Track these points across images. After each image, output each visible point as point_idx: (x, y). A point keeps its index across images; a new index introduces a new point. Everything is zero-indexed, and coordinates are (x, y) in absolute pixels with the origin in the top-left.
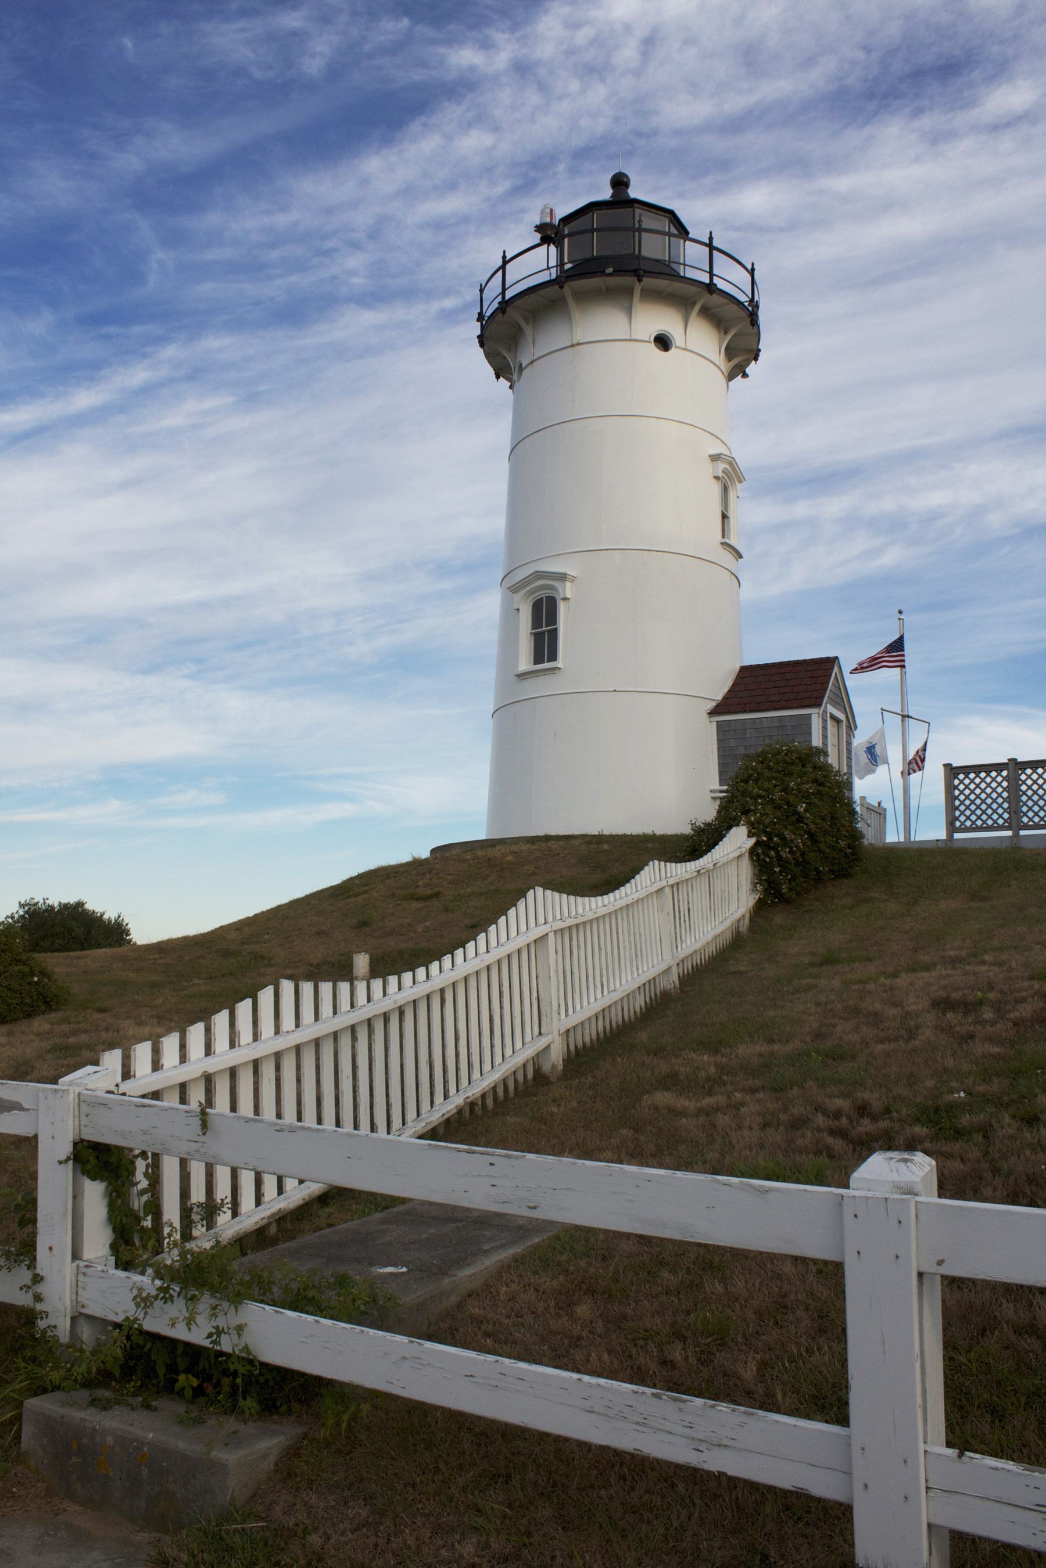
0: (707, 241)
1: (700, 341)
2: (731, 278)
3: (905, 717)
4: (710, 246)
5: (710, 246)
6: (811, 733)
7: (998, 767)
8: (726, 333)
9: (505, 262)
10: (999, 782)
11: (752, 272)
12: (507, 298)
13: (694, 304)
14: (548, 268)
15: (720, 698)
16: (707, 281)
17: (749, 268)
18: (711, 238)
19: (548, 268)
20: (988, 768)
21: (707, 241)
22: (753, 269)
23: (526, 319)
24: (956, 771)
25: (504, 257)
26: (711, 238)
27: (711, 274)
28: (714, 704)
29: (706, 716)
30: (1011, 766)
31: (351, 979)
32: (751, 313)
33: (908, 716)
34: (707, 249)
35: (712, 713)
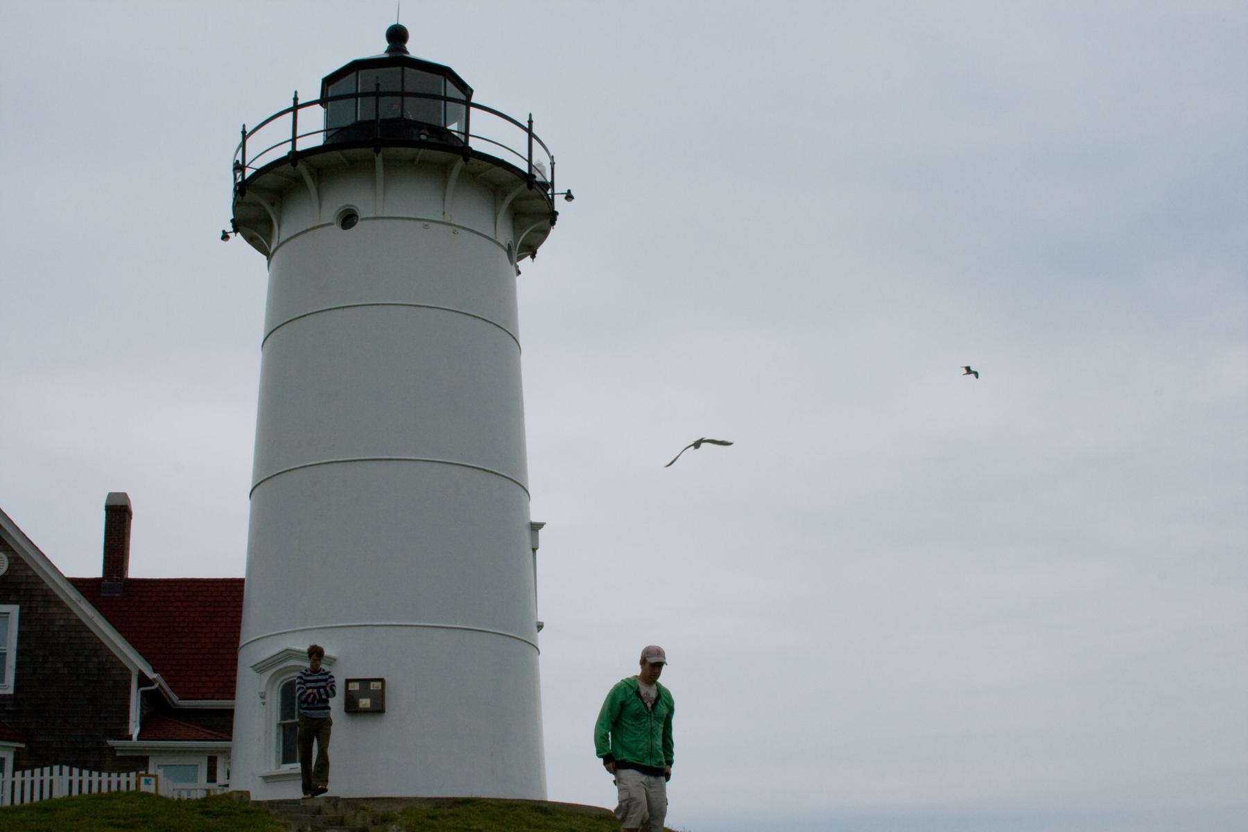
5: (529, 131)
9: (296, 108)
12: (299, 148)
13: (505, 195)
16: (526, 171)
18: (530, 122)
25: (296, 99)
26: (530, 122)
27: (530, 161)
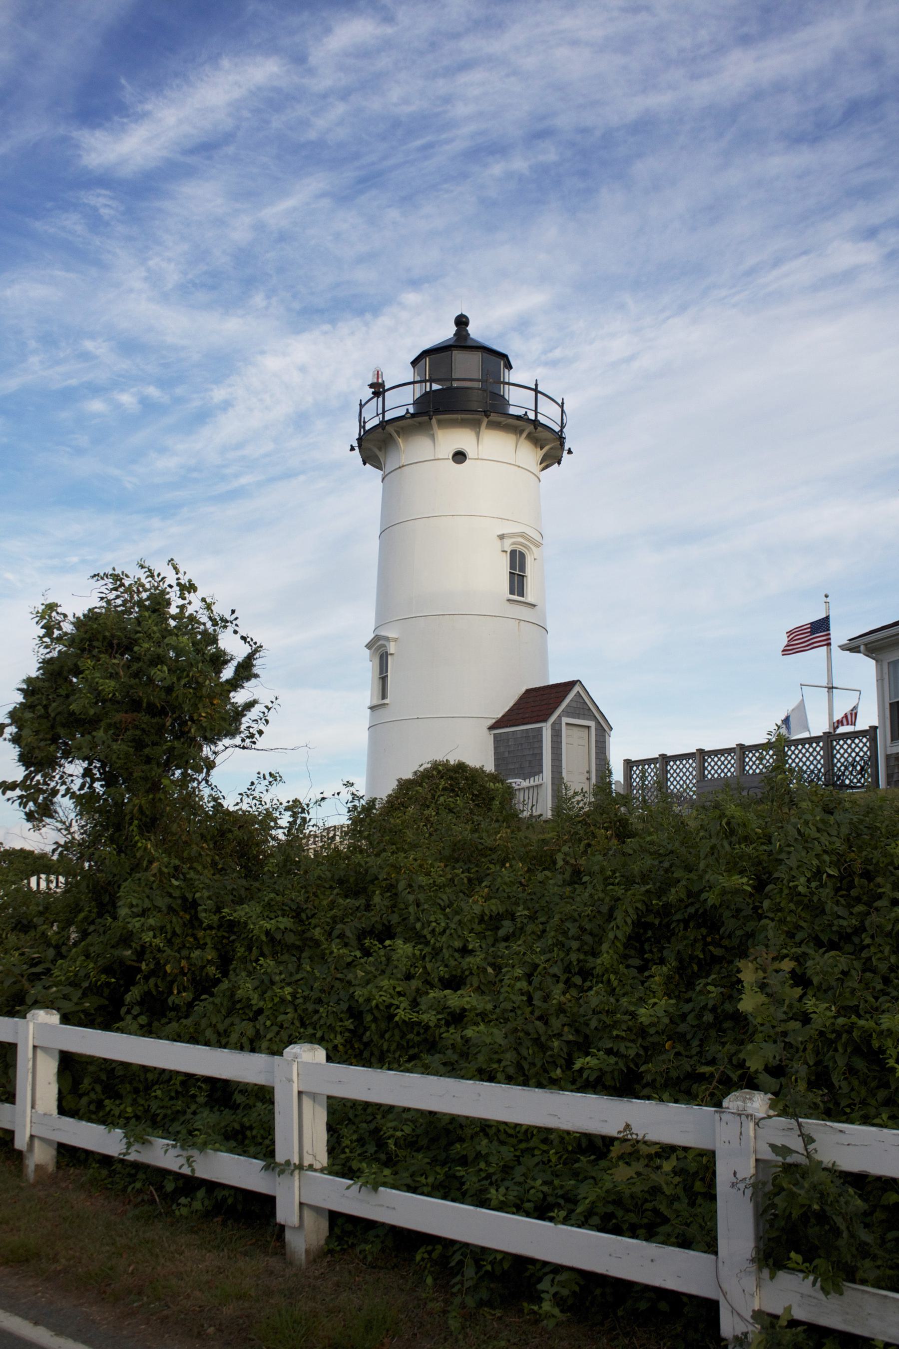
0: (534, 387)
1: (528, 455)
2: (549, 414)
3: (831, 688)
4: (536, 390)
5: (536, 390)
6: (542, 741)
7: (729, 751)
8: (541, 448)
10: (732, 760)
11: (562, 406)
14: (378, 415)
15: (500, 716)
17: (560, 402)
18: (536, 385)
19: (378, 415)
20: (722, 752)
21: (534, 387)
22: (563, 403)
23: (380, 449)
24: (631, 764)
25: (361, 404)
26: (536, 385)
28: (494, 721)
29: (487, 731)
30: (738, 751)
31: (895, 811)
32: (560, 438)
33: (833, 688)
34: (534, 393)
35: (491, 728)
